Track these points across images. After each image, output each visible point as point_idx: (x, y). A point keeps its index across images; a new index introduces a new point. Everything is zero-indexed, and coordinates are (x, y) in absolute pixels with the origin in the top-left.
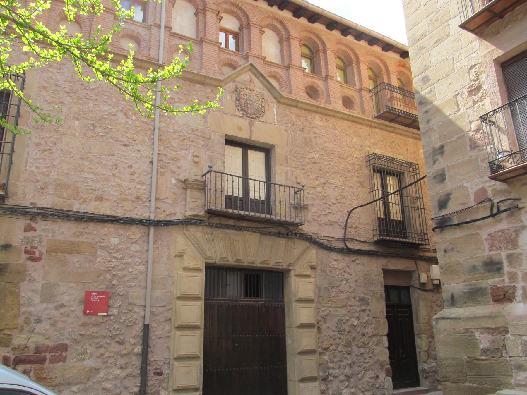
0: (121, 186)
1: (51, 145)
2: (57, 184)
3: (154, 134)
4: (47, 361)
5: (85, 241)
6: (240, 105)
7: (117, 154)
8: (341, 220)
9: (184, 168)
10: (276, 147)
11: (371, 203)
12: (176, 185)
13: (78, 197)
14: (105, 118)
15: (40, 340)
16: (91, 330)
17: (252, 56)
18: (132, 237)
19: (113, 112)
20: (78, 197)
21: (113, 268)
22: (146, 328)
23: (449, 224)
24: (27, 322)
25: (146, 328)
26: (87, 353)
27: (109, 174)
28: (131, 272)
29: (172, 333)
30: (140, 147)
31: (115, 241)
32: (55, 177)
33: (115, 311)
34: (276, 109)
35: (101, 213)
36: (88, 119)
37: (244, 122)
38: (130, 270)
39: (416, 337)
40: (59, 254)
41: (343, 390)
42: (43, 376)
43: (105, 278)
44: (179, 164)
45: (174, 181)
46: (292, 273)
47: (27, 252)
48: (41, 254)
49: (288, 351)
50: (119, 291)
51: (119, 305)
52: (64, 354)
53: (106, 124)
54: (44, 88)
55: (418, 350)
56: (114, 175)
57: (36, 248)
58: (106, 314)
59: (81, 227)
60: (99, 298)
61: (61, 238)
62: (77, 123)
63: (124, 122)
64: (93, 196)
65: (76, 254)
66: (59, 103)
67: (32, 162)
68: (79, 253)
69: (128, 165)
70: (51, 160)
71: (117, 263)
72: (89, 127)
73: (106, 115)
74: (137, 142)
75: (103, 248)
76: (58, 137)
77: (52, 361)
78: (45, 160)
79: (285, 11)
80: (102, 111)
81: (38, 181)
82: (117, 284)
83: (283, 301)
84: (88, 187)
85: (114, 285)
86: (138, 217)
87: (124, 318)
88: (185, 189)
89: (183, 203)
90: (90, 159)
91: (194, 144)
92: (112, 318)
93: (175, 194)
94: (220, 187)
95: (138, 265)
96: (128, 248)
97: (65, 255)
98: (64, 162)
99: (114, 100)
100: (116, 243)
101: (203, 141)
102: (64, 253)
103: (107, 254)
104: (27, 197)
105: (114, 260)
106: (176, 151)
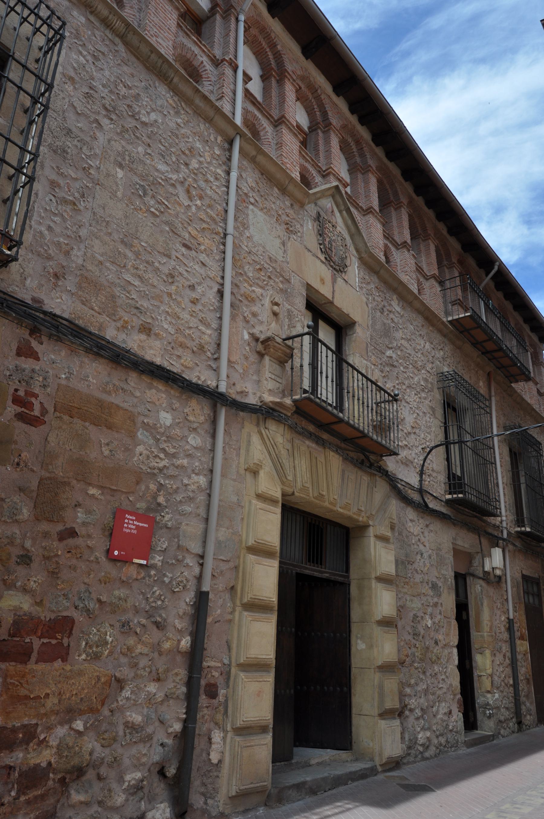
0: (179, 318)
1: (76, 195)
2: (81, 275)
3: (224, 244)
4: (34, 656)
5: (121, 405)
6: (325, 245)
7: (175, 258)
8: (416, 461)
9: (260, 318)
10: (357, 325)
12: (249, 345)
13: (115, 315)
14: (160, 183)
15: (26, 607)
16: (116, 593)
17: (334, 175)
18: (191, 418)
19: (171, 179)
20: (115, 315)
21: (161, 470)
22: (202, 600)
23: (422, 501)
25: (202, 600)
26: (107, 643)
27: (162, 288)
28: (186, 485)
29: (237, 614)
30: (203, 257)
31: (166, 418)
32: (80, 261)
33: (157, 559)
34: (358, 267)
35: (148, 358)
36: (135, 173)
37: (326, 272)
38: (186, 481)
39: (473, 652)
40: (75, 420)
41: (419, 733)
42: (23, 692)
43: (148, 488)
44: (255, 309)
45: (246, 337)
46: (371, 531)
47: (17, 400)
48: (44, 411)
49: (356, 662)
50: (166, 519)
51: (164, 546)
52: (65, 641)
53: (162, 196)
54: (71, 79)
55: (476, 673)
56: (170, 295)
57: (36, 396)
58: (144, 562)
59: (117, 376)
60: (137, 526)
61: (81, 387)
62: (120, 174)
63: (186, 204)
64: (136, 322)
65: (105, 429)
66: (93, 122)
67: (43, 215)
69: (188, 283)
70: (75, 224)
71: (165, 462)
72: (137, 189)
73: (162, 179)
74: (203, 248)
75: (146, 426)
76: (90, 185)
77: (41, 659)
78: (64, 220)
80: (157, 170)
81: (49, 258)
82: (164, 504)
83: (348, 577)
84: (130, 301)
85: (159, 504)
87: (170, 575)
88: (261, 355)
89: (255, 377)
90: (136, 249)
91: (271, 282)
92: (153, 572)
93: (247, 358)
94: (299, 365)
95: (197, 474)
96: (184, 438)
97: (87, 424)
98: (97, 238)
99: (174, 159)
100: (168, 424)
101: (282, 282)
102: (85, 421)
103: (151, 441)
104: (28, 282)
105: (162, 456)
106: (251, 286)
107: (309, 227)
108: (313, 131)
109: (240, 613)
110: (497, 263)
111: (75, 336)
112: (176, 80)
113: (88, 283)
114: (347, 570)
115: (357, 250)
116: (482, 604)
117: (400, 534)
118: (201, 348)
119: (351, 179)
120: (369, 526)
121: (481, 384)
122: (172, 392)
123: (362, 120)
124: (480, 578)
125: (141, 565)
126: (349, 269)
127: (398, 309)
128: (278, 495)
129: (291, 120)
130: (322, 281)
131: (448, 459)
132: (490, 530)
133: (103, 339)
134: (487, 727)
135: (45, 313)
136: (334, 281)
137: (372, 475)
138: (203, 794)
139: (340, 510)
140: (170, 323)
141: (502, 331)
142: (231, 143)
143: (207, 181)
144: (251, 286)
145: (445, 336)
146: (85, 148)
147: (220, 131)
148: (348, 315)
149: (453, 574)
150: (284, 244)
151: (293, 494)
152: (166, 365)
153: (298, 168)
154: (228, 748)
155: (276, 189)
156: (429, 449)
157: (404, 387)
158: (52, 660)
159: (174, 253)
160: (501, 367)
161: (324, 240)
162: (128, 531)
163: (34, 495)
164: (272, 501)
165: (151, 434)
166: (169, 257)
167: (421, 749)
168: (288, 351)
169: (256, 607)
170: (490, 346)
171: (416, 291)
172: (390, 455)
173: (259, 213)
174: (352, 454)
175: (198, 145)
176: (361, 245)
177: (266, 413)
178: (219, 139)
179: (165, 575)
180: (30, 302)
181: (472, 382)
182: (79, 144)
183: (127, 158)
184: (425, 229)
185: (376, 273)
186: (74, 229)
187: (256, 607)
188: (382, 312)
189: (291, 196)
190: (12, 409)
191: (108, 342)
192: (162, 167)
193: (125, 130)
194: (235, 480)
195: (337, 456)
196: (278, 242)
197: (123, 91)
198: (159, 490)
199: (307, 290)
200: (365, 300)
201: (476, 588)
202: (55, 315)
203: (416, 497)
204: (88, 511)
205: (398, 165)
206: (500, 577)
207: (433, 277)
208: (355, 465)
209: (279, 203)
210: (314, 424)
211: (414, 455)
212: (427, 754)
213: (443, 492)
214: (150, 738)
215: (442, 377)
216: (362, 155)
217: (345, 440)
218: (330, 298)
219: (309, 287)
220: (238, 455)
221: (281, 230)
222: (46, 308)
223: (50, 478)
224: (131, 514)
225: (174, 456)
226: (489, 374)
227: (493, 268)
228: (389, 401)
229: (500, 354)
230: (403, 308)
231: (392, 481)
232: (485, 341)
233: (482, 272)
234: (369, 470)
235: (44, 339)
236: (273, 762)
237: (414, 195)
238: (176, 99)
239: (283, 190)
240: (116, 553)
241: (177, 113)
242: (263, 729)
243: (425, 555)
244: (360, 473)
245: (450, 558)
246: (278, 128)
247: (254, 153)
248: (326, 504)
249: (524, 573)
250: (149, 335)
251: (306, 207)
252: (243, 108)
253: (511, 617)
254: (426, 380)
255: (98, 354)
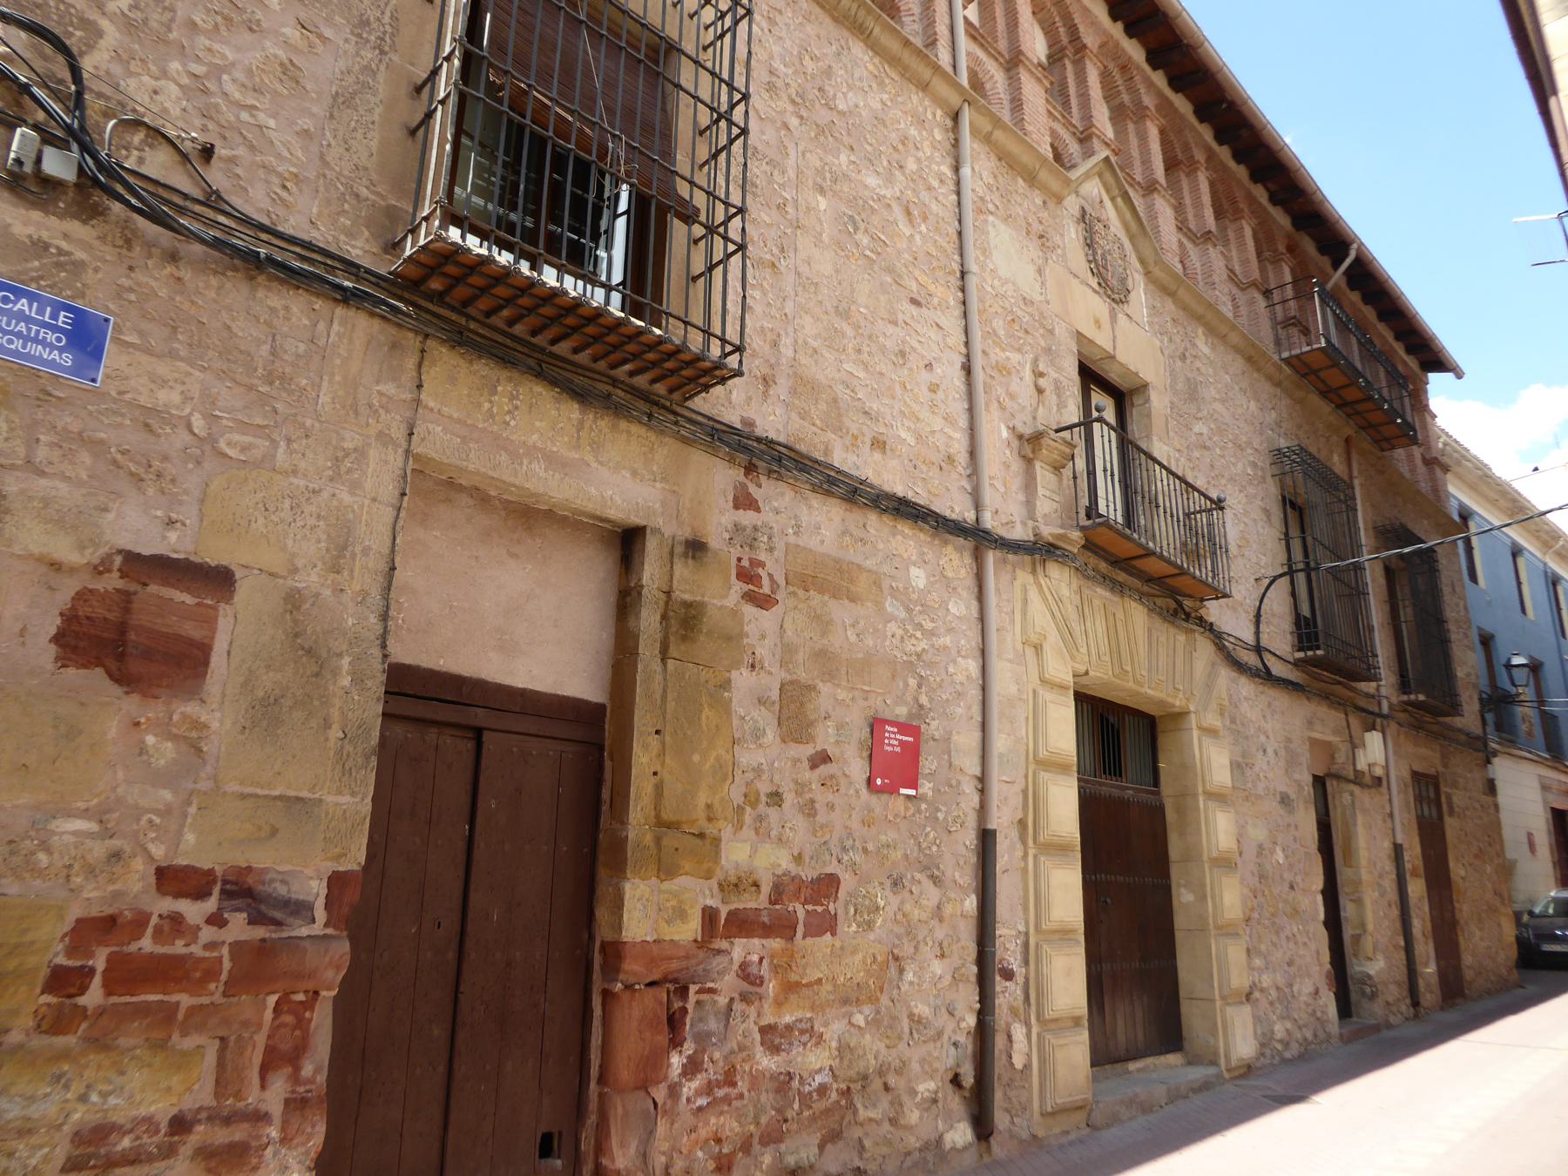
6: (1095, 261)
11: (973, 453)
24: (751, 799)
25: (986, 838)
33: (926, 787)
45: (1005, 433)
52: (831, 907)
57: (762, 564)
58: (912, 792)
60: (902, 743)
61: (812, 542)
62: (823, 203)
68: (853, 600)
71: (923, 645)
79: (1134, 41)
83: (1158, 793)
86: (954, 517)
92: (924, 806)
96: (944, 604)
107: (1072, 235)
108: (1055, 62)
109: (1035, 857)
110: (1355, 246)
111: (801, 470)
112: (877, 31)
113: (804, 386)
114: (1156, 783)
115: (1142, 261)
116: (1355, 825)
117: (1233, 721)
118: (950, 459)
119: (1116, 133)
120: (1188, 713)
121: (1336, 458)
122: (922, 536)
123: (1130, 31)
124: (1349, 781)
125: (908, 797)
126: (1132, 296)
127: (1206, 350)
128: (1070, 680)
129: (1029, 54)
130: (1098, 323)
131: (1293, 594)
132: (1362, 703)
133: (831, 467)
134: (1373, 1011)
135: (759, 440)
136: (1113, 318)
137: (1189, 631)
138: (1007, 1110)
139: (1150, 692)
140: (909, 429)
141: (1362, 358)
142: (956, 117)
143: (930, 188)
144: (1004, 350)
145: (1278, 384)
146: (776, 173)
147: (938, 101)
148: (1136, 374)
149: (1311, 779)
150: (1040, 271)
151: (1087, 673)
152: (910, 496)
153: (1048, 139)
154: (1034, 1049)
155: (1020, 181)
156: (1267, 581)
157: (1223, 482)
158: (820, 933)
159: (900, 317)
160: (1367, 427)
161: (1095, 253)
162: (889, 749)
163: (777, 707)
164: (1063, 687)
165: (903, 604)
166: (895, 323)
167: (1279, 1047)
168: (1068, 450)
169: (1057, 849)
170: (1351, 394)
171: (1230, 315)
172: (1217, 598)
173: (1002, 227)
174: (1159, 601)
175: (913, 132)
176: (1148, 253)
177: (1041, 551)
178: (939, 112)
179: (938, 810)
180: (739, 426)
181: (1322, 457)
182: (768, 169)
183: (828, 175)
184: (1234, 202)
185: (1172, 294)
186: (779, 304)
187: (1057, 849)
188: (1183, 358)
189: (1044, 188)
190: (738, 587)
191: (839, 472)
192: (872, 181)
193: (821, 131)
194: (1011, 661)
195: (1141, 608)
196: (1031, 269)
197: (809, 65)
198: (920, 686)
199: (1079, 342)
200: (1158, 343)
201: (1342, 797)
202: (772, 441)
203: (1251, 659)
204: (840, 723)
205: (1188, 97)
206: (1379, 779)
207: (1254, 284)
208: (1165, 619)
209: (1028, 202)
210: (1106, 560)
211: (1244, 591)
212: (1288, 1055)
213: (1289, 649)
214: (940, 1034)
215: (1278, 455)
216: (1132, 90)
217: (1149, 579)
218: (1110, 349)
219: (1079, 335)
220: (1013, 621)
221: (1033, 251)
222: (759, 432)
223: (792, 682)
224: (892, 723)
225: (932, 633)
226: (1347, 441)
227: (1347, 255)
228: (1211, 510)
229: (1368, 405)
230: (1213, 348)
231: (1217, 636)
232: (1342, 387)
233: (1325, 262)
234: (1185, 624)
235: (763, 479)
236: (1093, 1065)
237: (1214, 145)
238: (877, 60)
239: (1032, 180)
240: (879, 782)
241: (881, 84)
242: (1076, 1021)
243: (1270, 751)
244: (1172, 630)
245: (1305, 757)
246: (1013, 72)
247: (988, 128)
248: (1131, 685)
249: (1416, 768)
250: (884, 452)
251: (1065, 203)
252: (968, 54)
253: (1399, 841)
254: (1254, 465)
255: (828, 493)
